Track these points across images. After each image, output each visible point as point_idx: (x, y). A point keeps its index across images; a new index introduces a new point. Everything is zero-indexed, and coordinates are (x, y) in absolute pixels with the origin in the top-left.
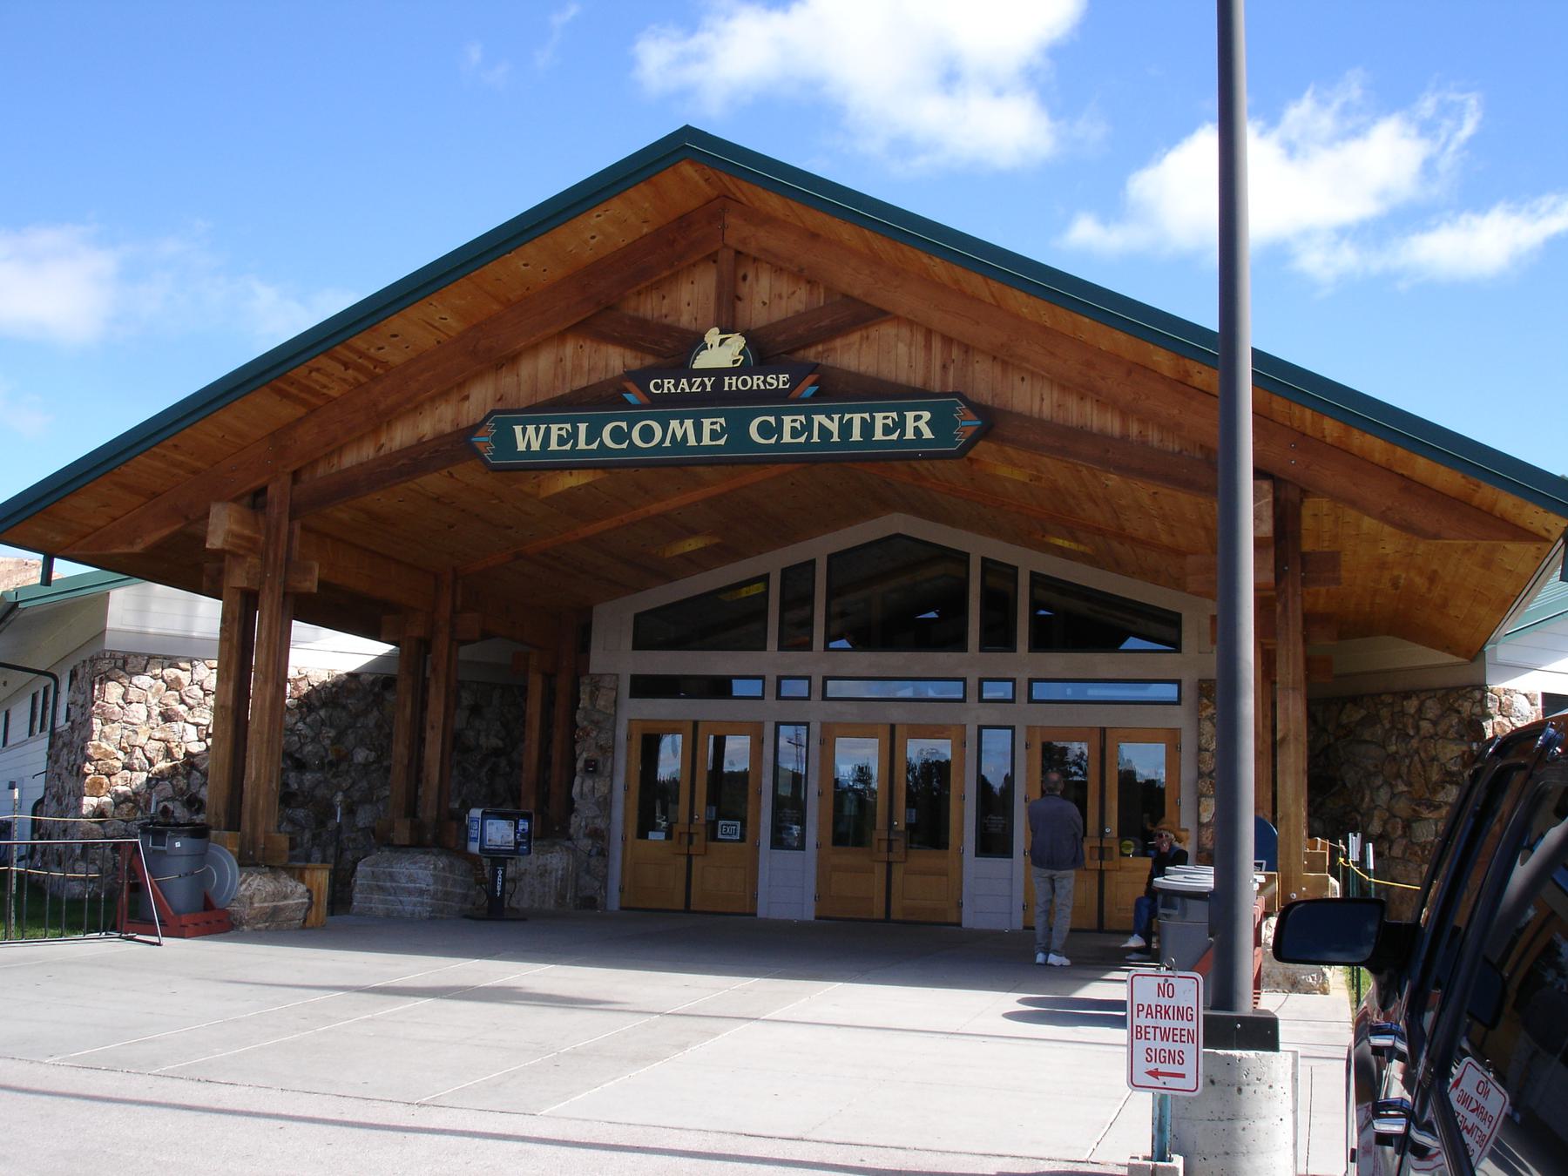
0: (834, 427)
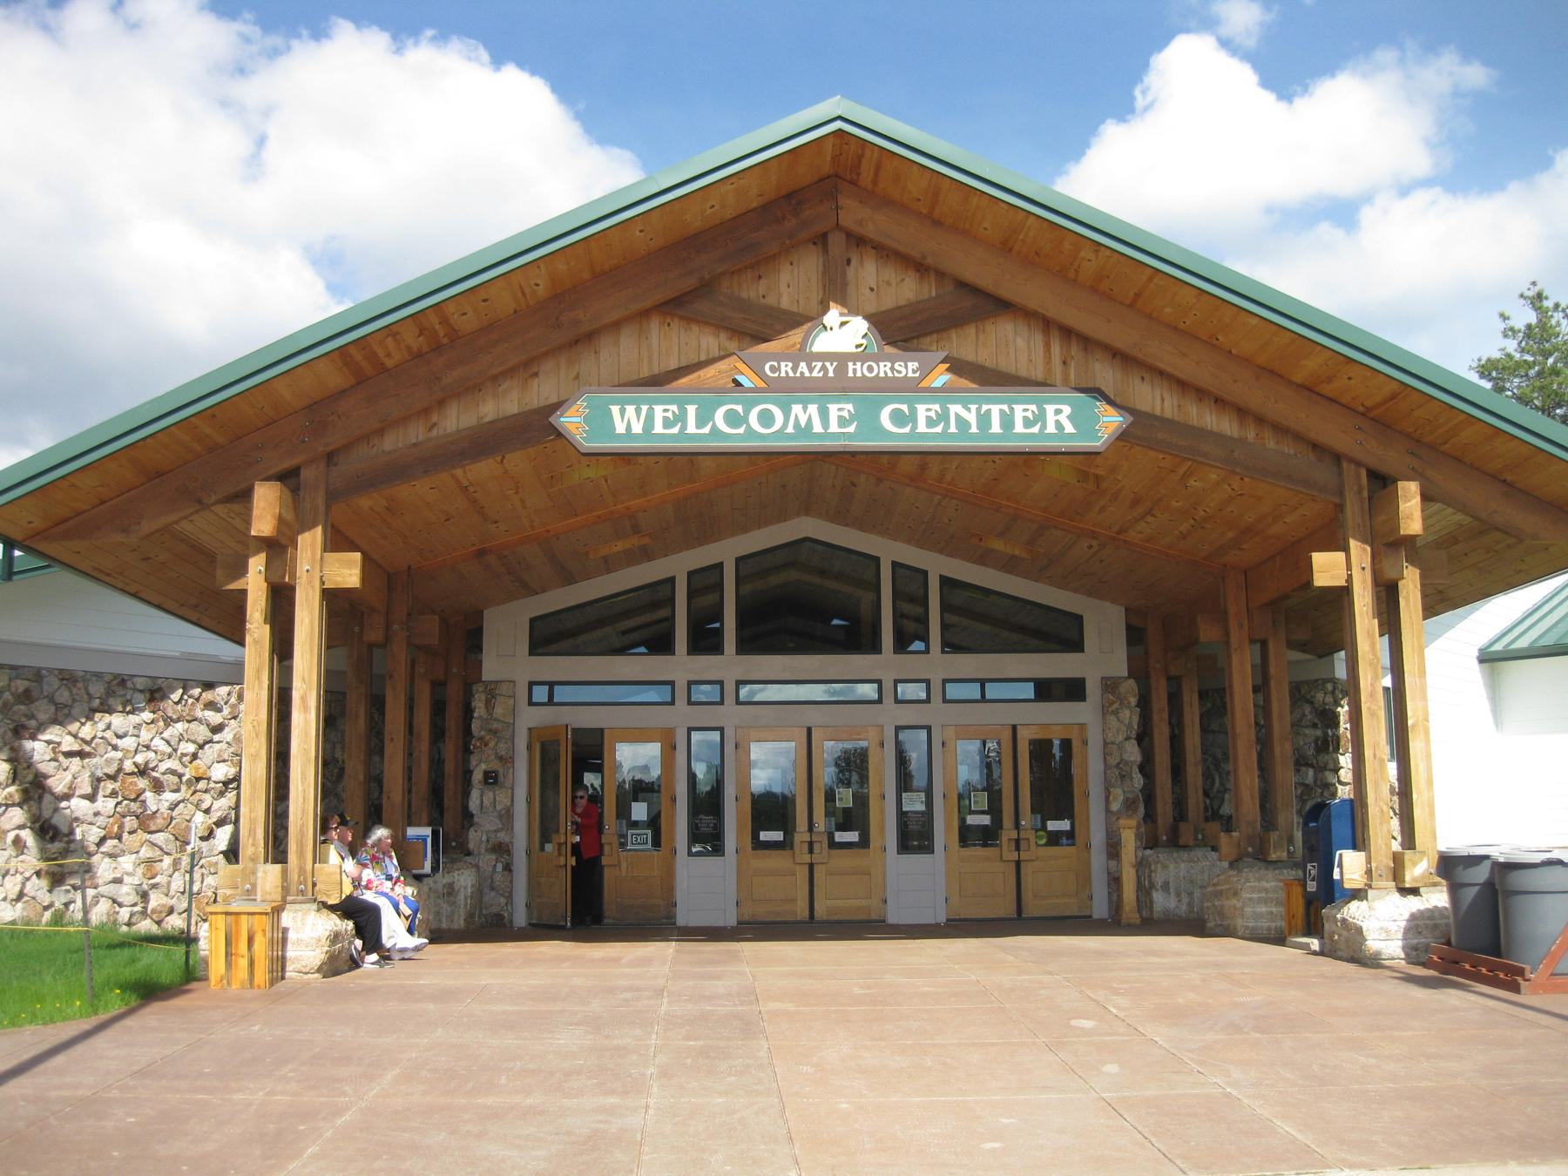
0: (971, 417)
